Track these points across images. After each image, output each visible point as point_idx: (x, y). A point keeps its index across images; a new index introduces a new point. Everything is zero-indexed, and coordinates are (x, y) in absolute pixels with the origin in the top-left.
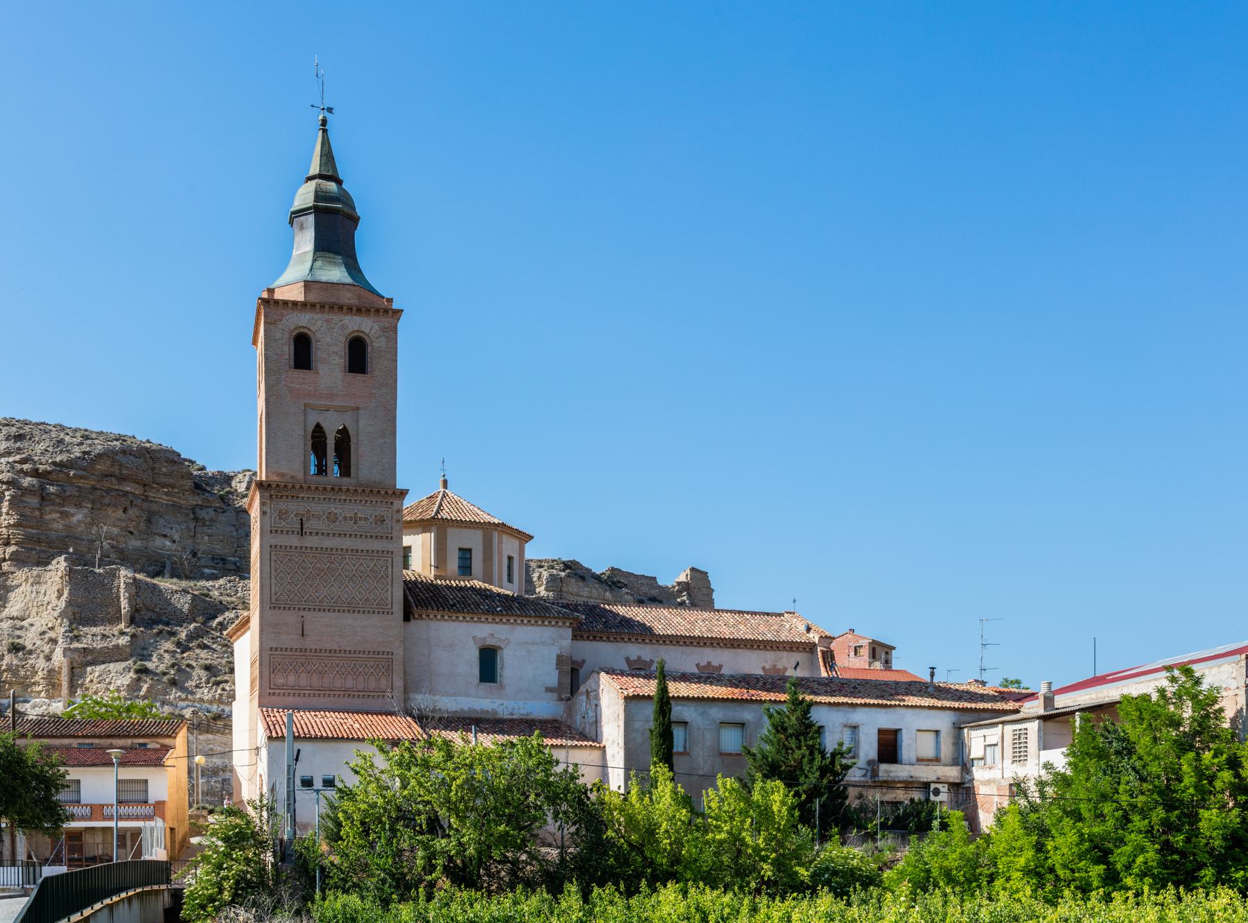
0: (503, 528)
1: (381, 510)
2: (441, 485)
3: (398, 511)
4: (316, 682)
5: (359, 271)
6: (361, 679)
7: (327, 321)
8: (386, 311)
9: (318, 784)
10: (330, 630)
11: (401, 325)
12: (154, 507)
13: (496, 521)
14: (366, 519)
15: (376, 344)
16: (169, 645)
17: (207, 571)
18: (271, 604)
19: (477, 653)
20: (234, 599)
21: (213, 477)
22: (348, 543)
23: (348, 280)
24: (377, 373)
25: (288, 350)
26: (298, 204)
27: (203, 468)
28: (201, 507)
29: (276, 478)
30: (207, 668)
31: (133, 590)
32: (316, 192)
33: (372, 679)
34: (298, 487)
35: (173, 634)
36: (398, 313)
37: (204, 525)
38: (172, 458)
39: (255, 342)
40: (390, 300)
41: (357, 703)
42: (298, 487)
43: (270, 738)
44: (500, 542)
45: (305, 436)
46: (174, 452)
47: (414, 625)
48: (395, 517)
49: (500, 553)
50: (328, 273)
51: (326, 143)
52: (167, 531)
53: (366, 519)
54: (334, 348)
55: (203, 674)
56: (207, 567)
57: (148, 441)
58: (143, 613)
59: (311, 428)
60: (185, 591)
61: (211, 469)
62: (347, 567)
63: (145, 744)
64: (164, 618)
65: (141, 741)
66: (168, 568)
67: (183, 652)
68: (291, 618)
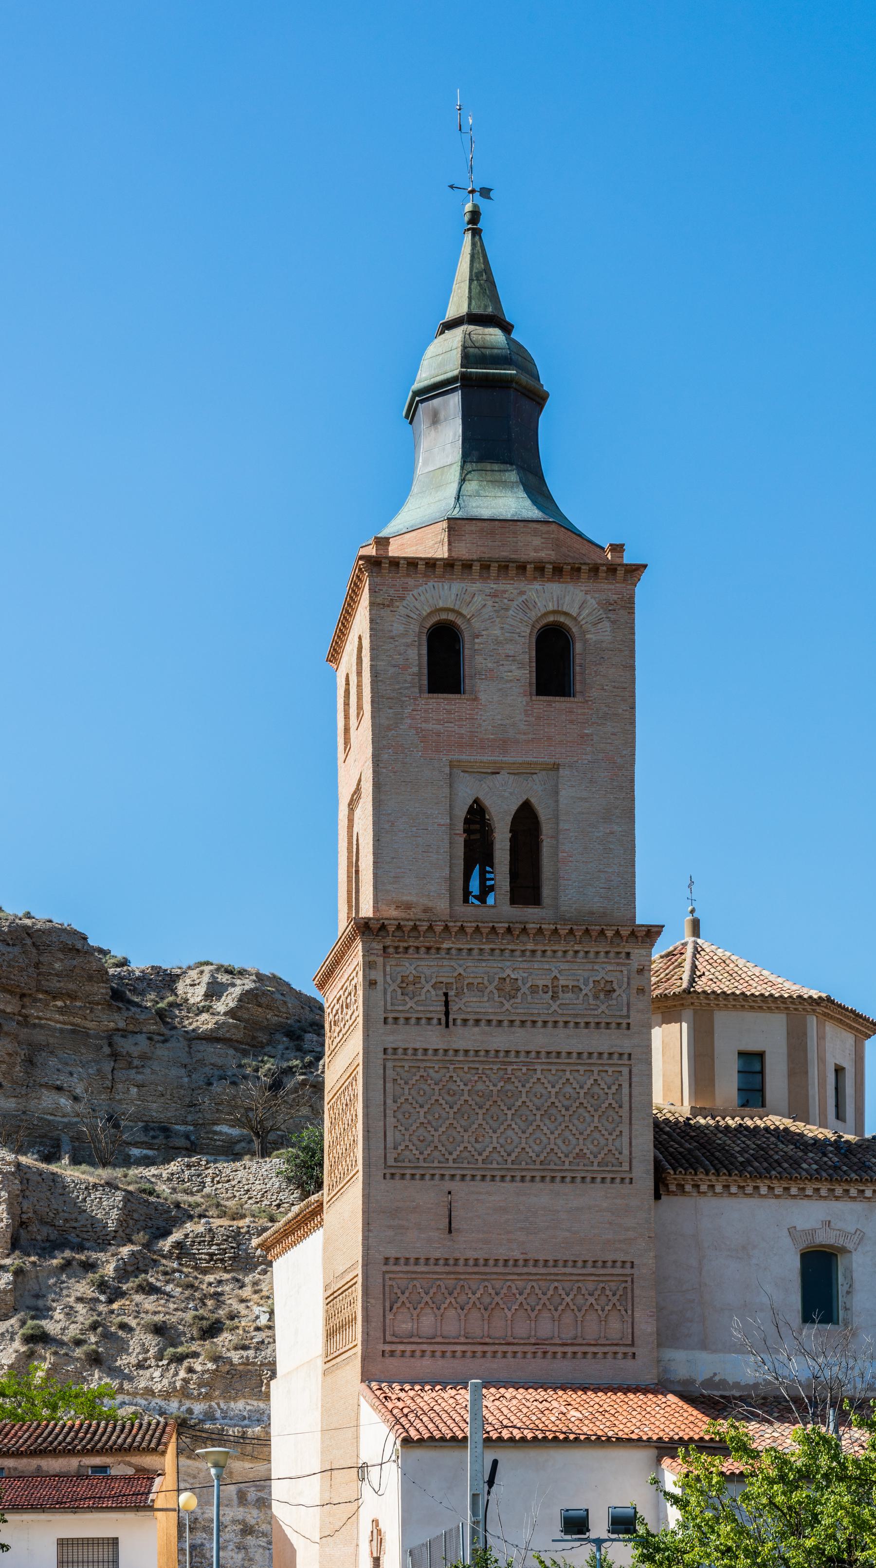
0: (827, 1008)
1: (606, 970)
2: (687, 929)
3: (641, 971)
4: (476, 1326)
5: (549, 497)
6: (568, 1318)
7: (494, 595)
8: (612, 569)
9: (599, 1527)
10: (504, 1218)
11: (643, 591)
12: (39, 1037)
13: (815, 994)
14: (576, 989)
15: (591, 634)
16: (83, 1288)
17: (135, 1152)
18: (387, 1168)
19: (795, 1263)
20: (198, 1198)
21: (143, 977)
22: (539, 1040)
23: (534, 513)
24: (594, 693)
25: (415, 656)
26: (425, 376)
27: (124, 963)
28: (125, 1033)
29: (393, 913)
30: (159, 1330)
31: (17, 1185)
32: (464, 347)
33: (568, 1318)
34: (439, 929)
35: (89, 1266)
36: (636, 570)
37: (130, 1066)
38: (72, 945)
39: (334, 655)
40: (617, 548)
41: (562, 1368)
42: (439, 929)
43: (407, 1441)
44: (821, 1037)
45: (451, 826)
46: (75, 933)
47: (677, 1208)
48: (636, 982)
49: (822, 1060)
50: (501, 501)
51: (479, 255)
52: (62, 1079)
53: (576, 989)
54: (510, 649)
55: (152, 1341)
56: (136, 1144)
57: (28, 916)
58: (34, 1228)
59: (461, 813)
60: (110, 1185)
61: (139, 964)
62: (539, 1088)
63: (104, 1468)
64: (73, 1238)
65: (97, 1461)
66: (66, 1146)
67: (111, 1301)
68: (426, 1197)
